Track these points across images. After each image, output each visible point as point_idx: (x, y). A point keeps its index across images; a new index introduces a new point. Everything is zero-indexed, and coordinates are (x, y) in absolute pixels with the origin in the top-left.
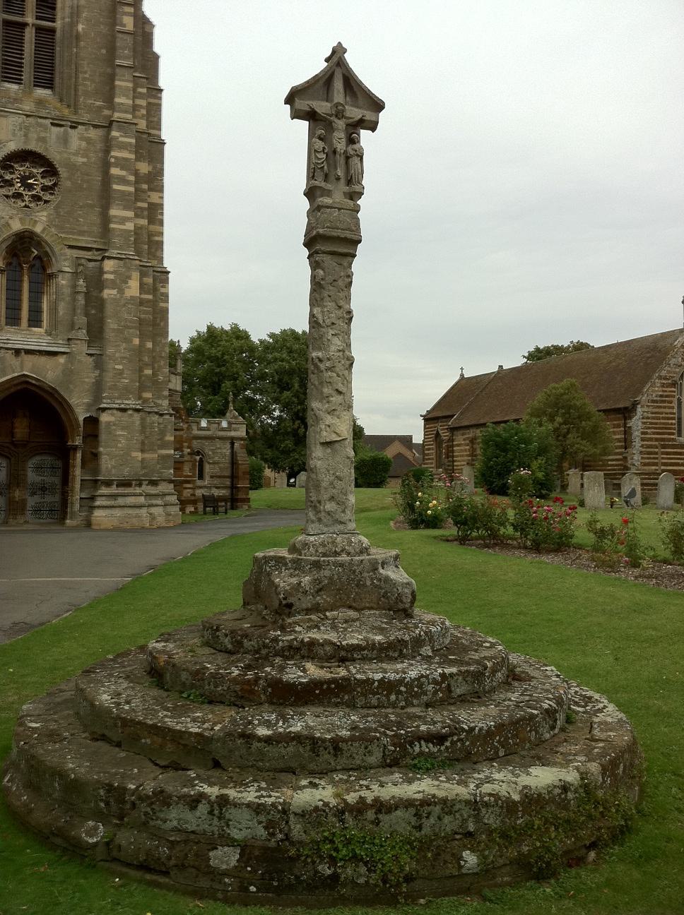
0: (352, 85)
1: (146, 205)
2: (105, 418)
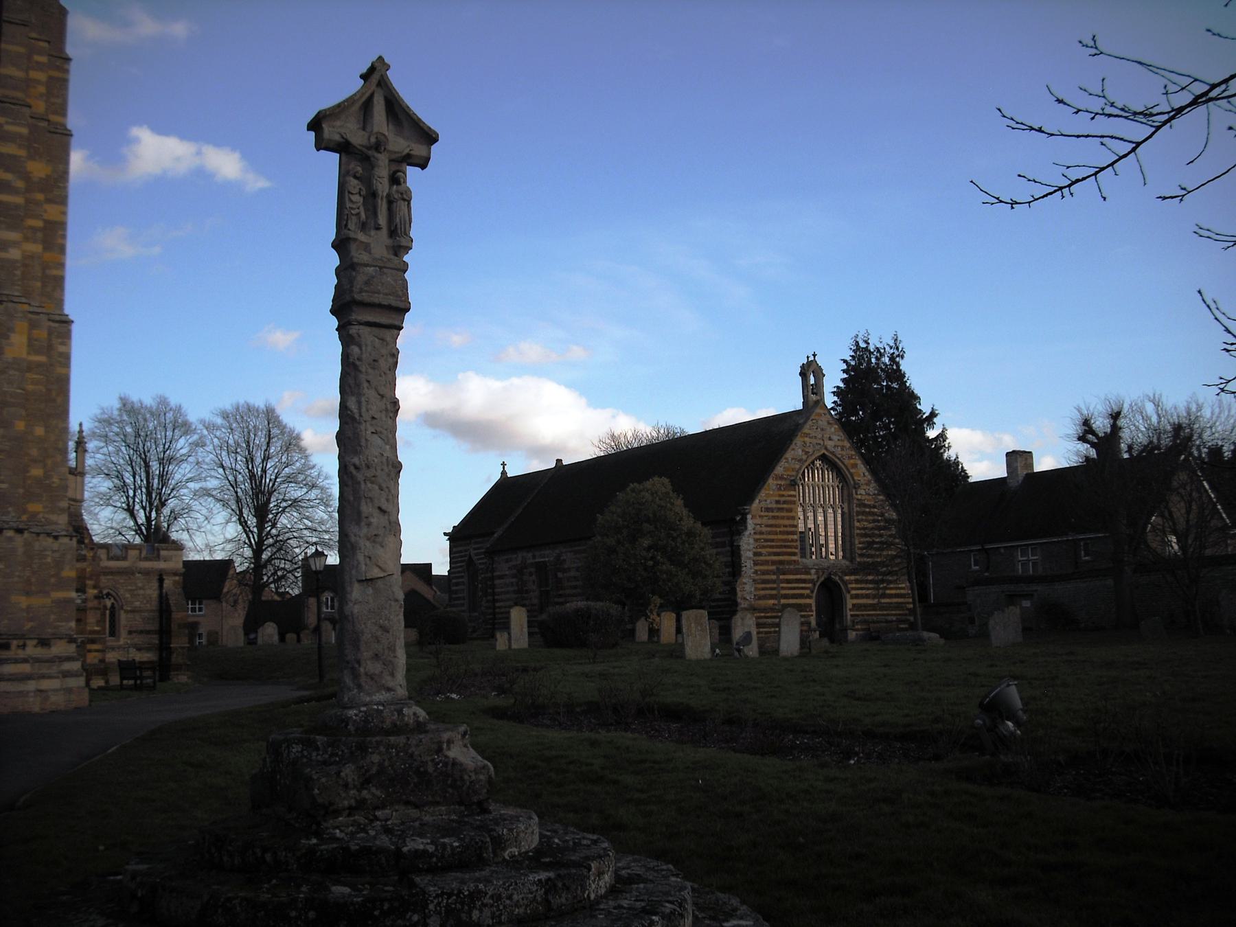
0: (397, 110)
1: (40, 224)
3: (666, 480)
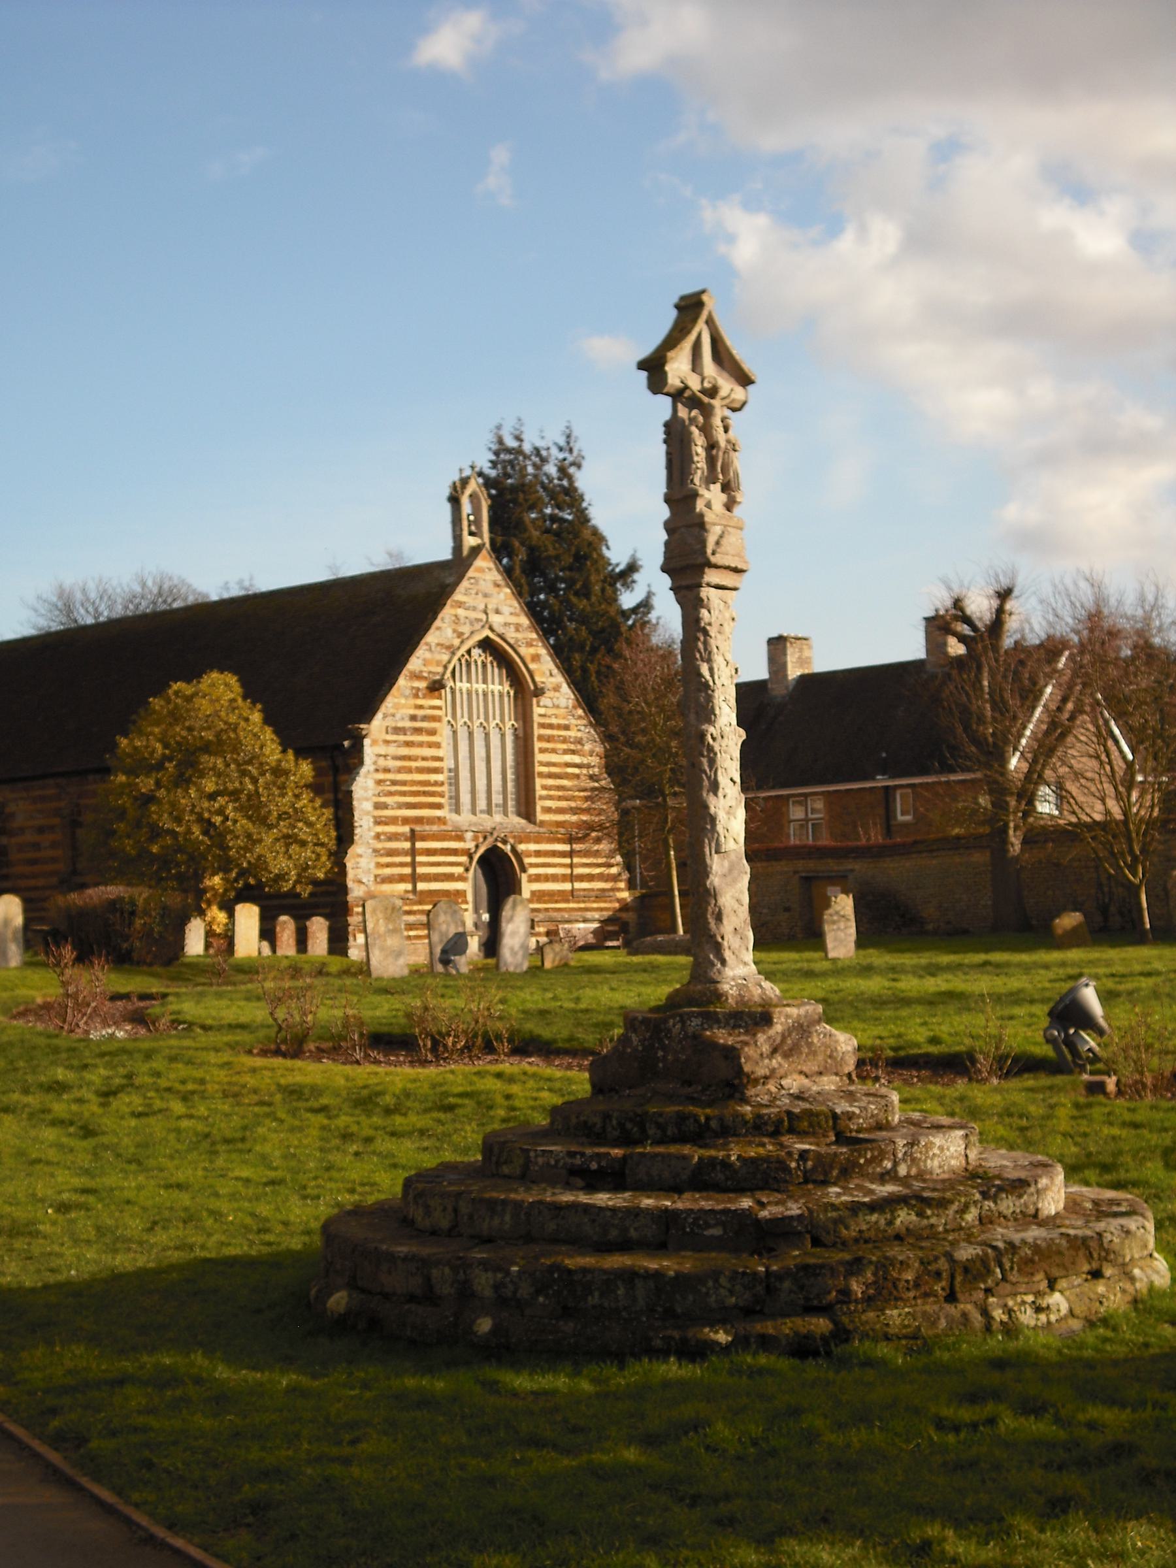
3: (233, 680)
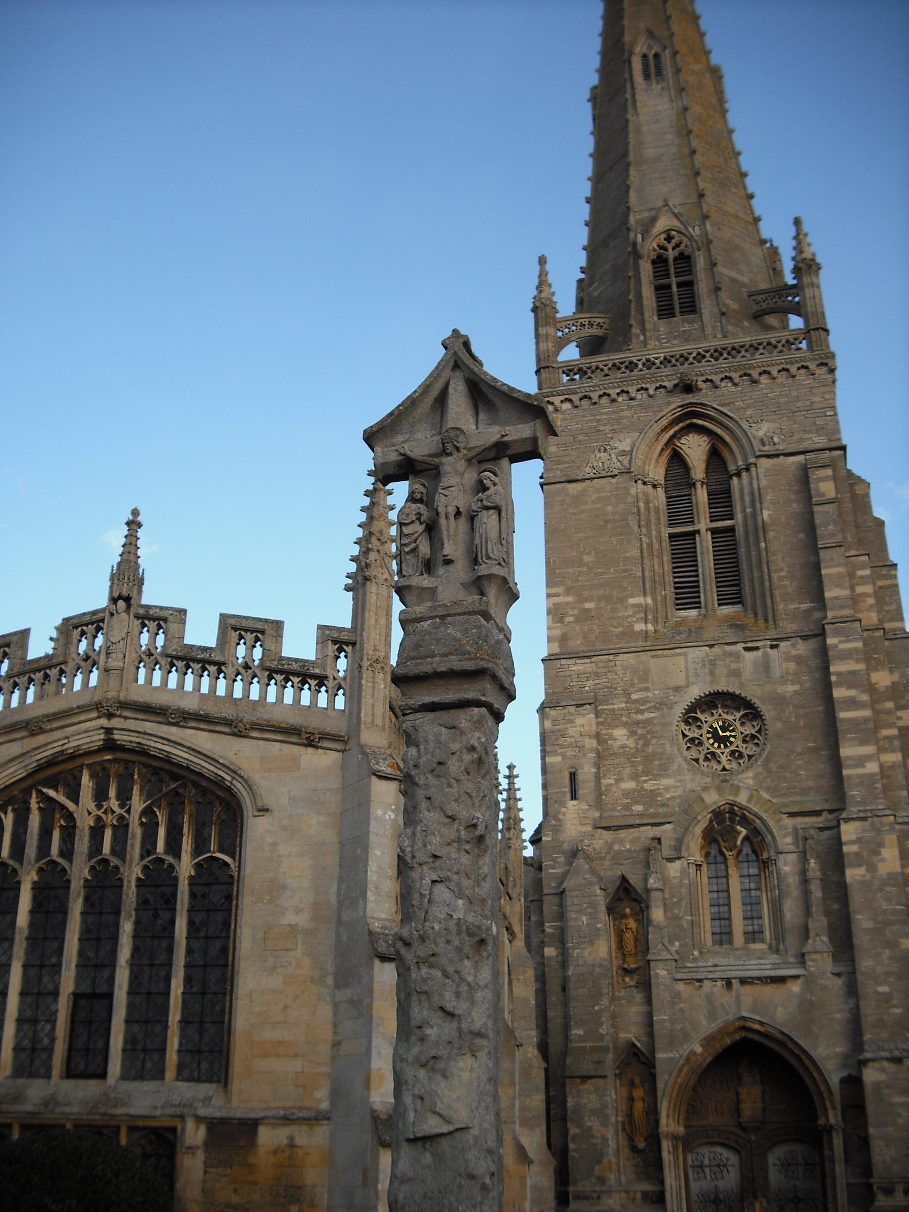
1: (895, 732)
2: (870, 1075)
